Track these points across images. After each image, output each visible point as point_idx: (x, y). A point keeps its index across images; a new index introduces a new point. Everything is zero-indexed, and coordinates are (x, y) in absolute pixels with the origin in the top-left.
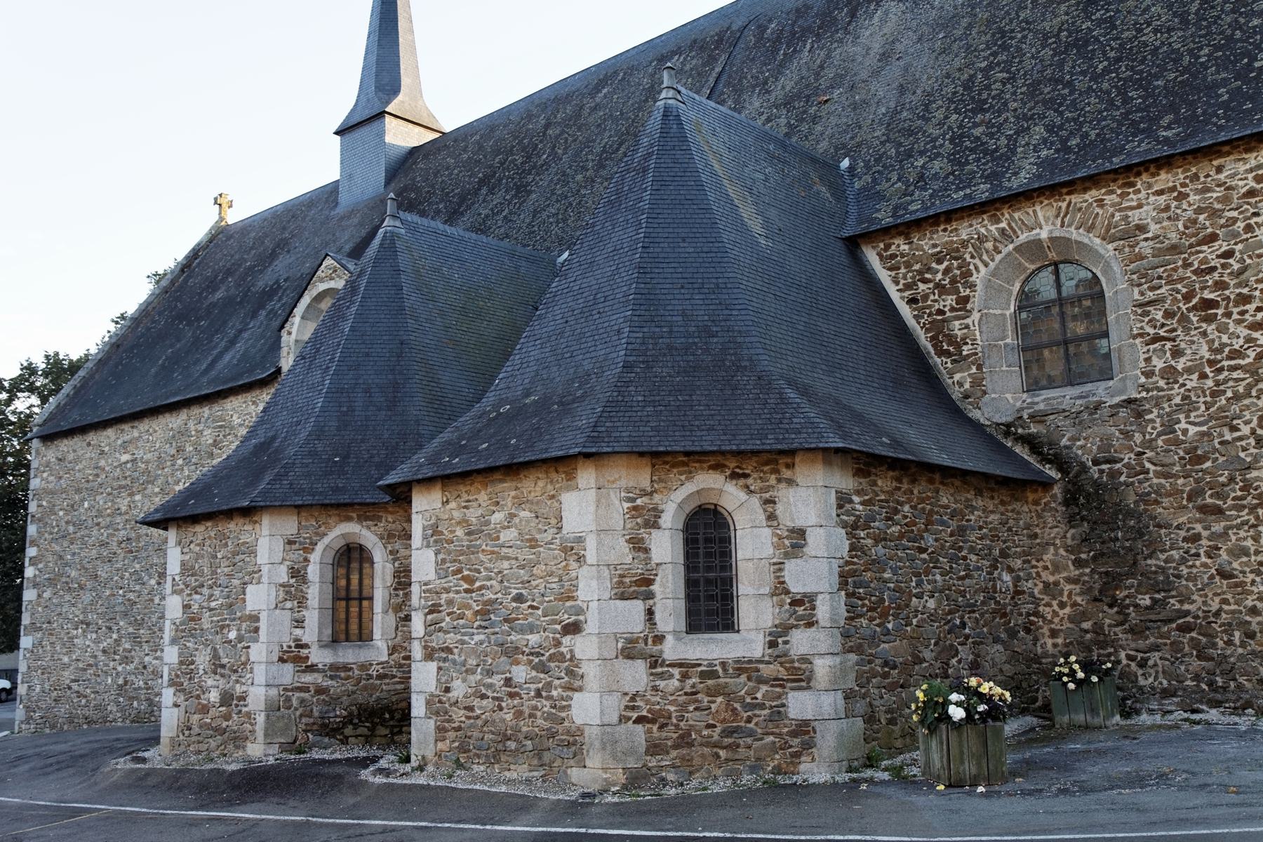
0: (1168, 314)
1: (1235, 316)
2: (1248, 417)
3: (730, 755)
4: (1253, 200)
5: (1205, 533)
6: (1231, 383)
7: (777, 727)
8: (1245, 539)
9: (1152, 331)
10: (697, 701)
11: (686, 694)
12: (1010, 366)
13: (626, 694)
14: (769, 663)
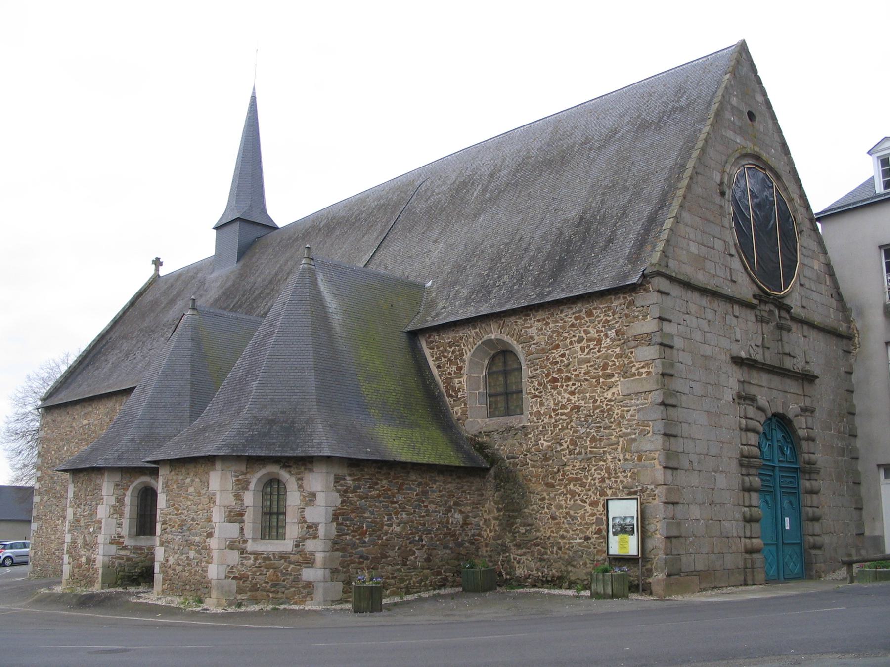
0: (540, 384)
1: (564, 387)
2: (566, 439)
3: (274, 596)
4: (573, 329)
5: (547, 497)
6: (561, 422)
7: (297, 584)
8: (561, 501)
9: (533, 392)
10: (260, 570)
11: (256, 567)
12: (481, 404)
13: (229, 566)
14: (294, 554)
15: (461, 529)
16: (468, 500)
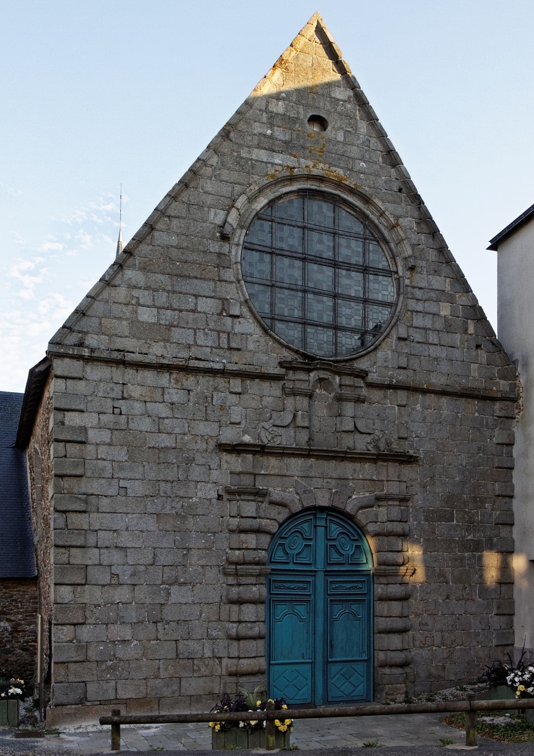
15: (10, 636)
16: (18, 609)
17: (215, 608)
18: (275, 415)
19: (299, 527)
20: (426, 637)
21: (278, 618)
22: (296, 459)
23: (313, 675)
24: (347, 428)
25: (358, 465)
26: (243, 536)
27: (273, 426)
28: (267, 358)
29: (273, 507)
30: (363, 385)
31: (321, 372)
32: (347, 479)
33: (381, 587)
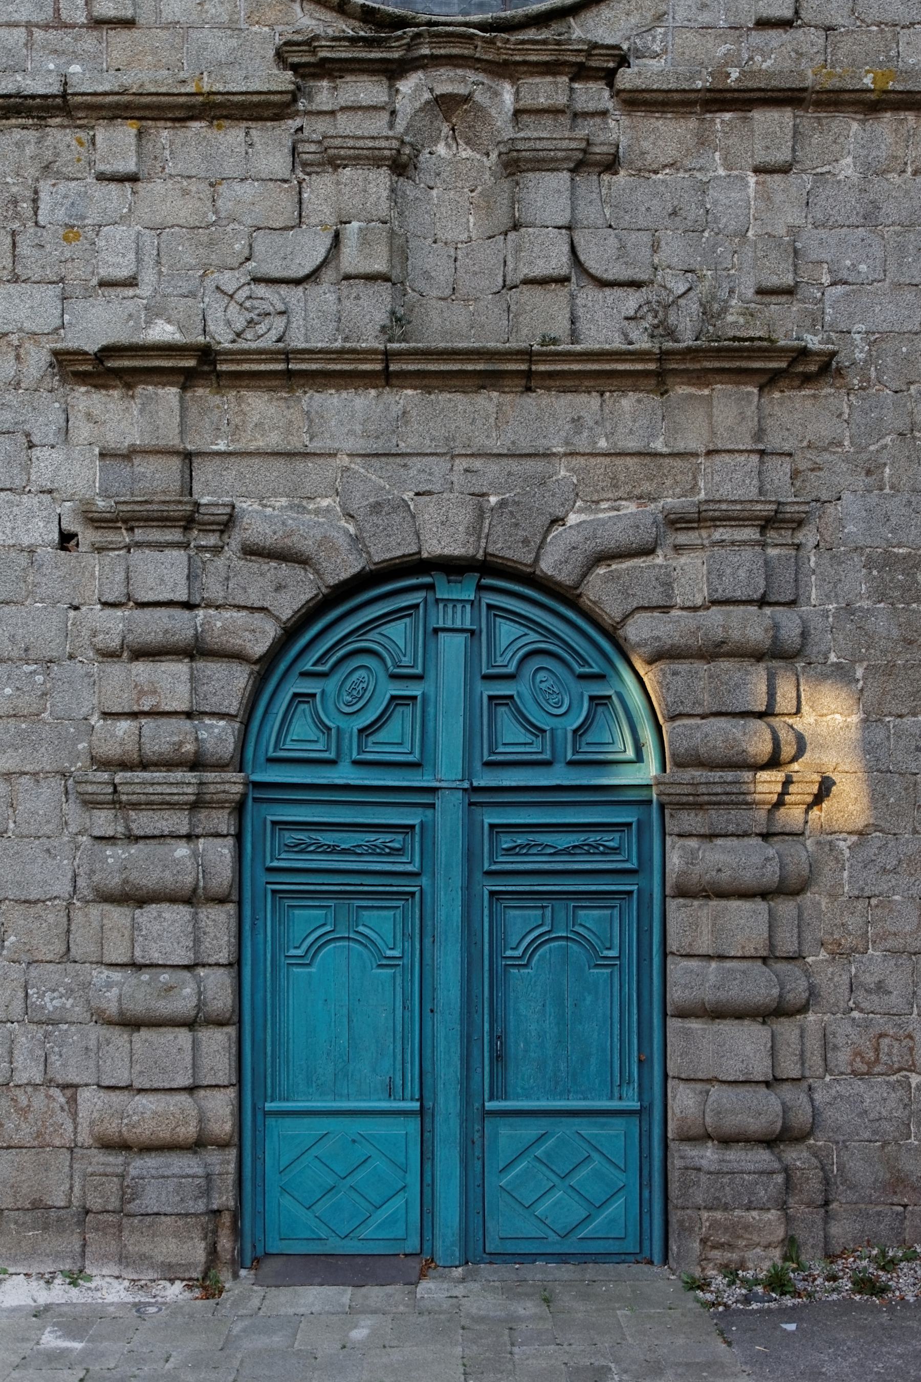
17: (53, 917)
18: (262, 243)
19: (373, 635)
20: (881, 1036)
21: (299, 952)
22: (344, 394)
23: (426, 1156)
24: (540, 269)
25: (594, 401)
26: (142, 669)
27: (256, 280)
28: (234, 42)
29: (256, 565)
30: (610, 105)
31: (444, 72)
32: (547, 455)
33: (683, 847)
